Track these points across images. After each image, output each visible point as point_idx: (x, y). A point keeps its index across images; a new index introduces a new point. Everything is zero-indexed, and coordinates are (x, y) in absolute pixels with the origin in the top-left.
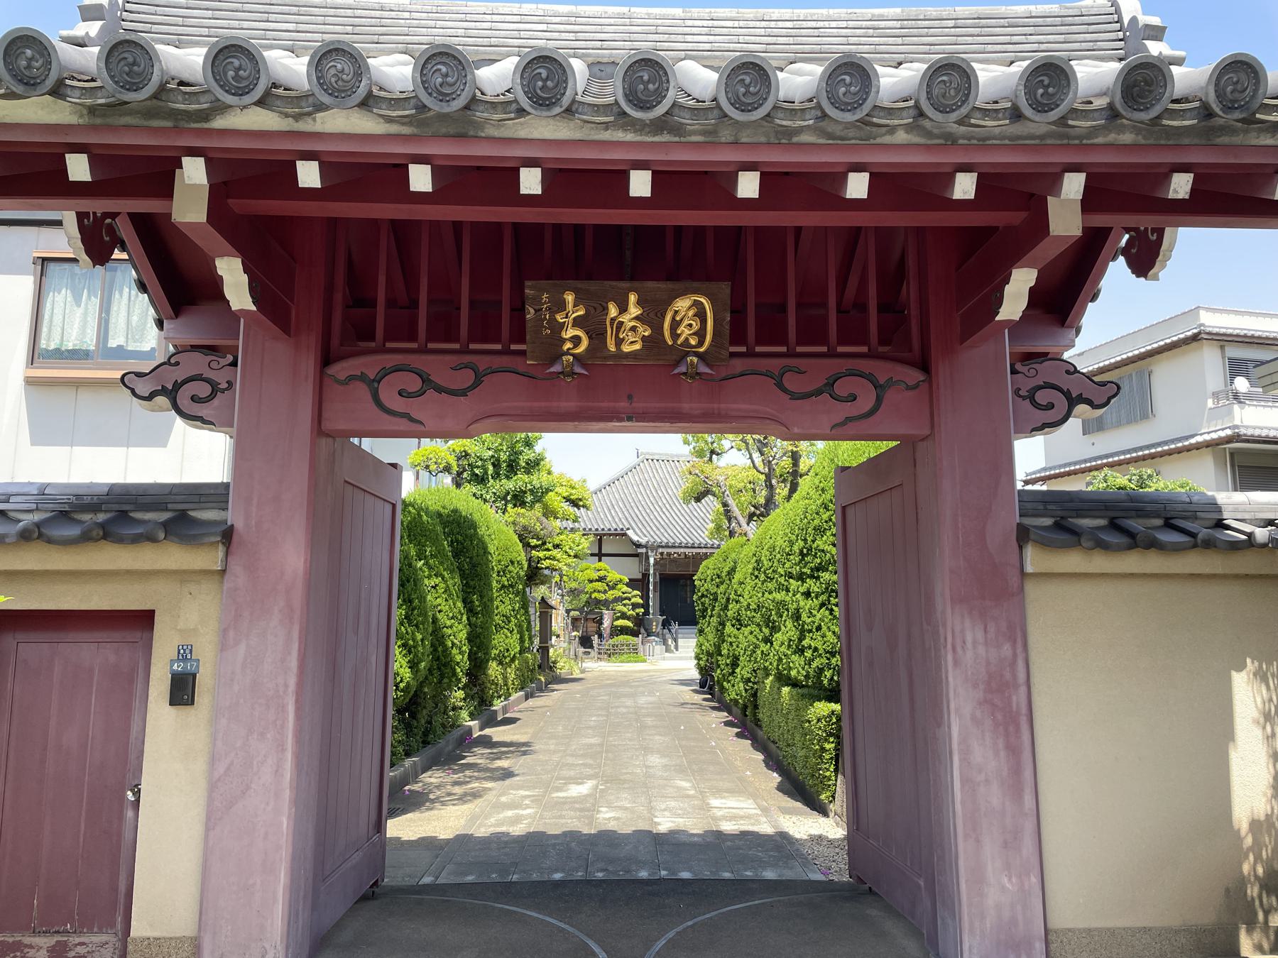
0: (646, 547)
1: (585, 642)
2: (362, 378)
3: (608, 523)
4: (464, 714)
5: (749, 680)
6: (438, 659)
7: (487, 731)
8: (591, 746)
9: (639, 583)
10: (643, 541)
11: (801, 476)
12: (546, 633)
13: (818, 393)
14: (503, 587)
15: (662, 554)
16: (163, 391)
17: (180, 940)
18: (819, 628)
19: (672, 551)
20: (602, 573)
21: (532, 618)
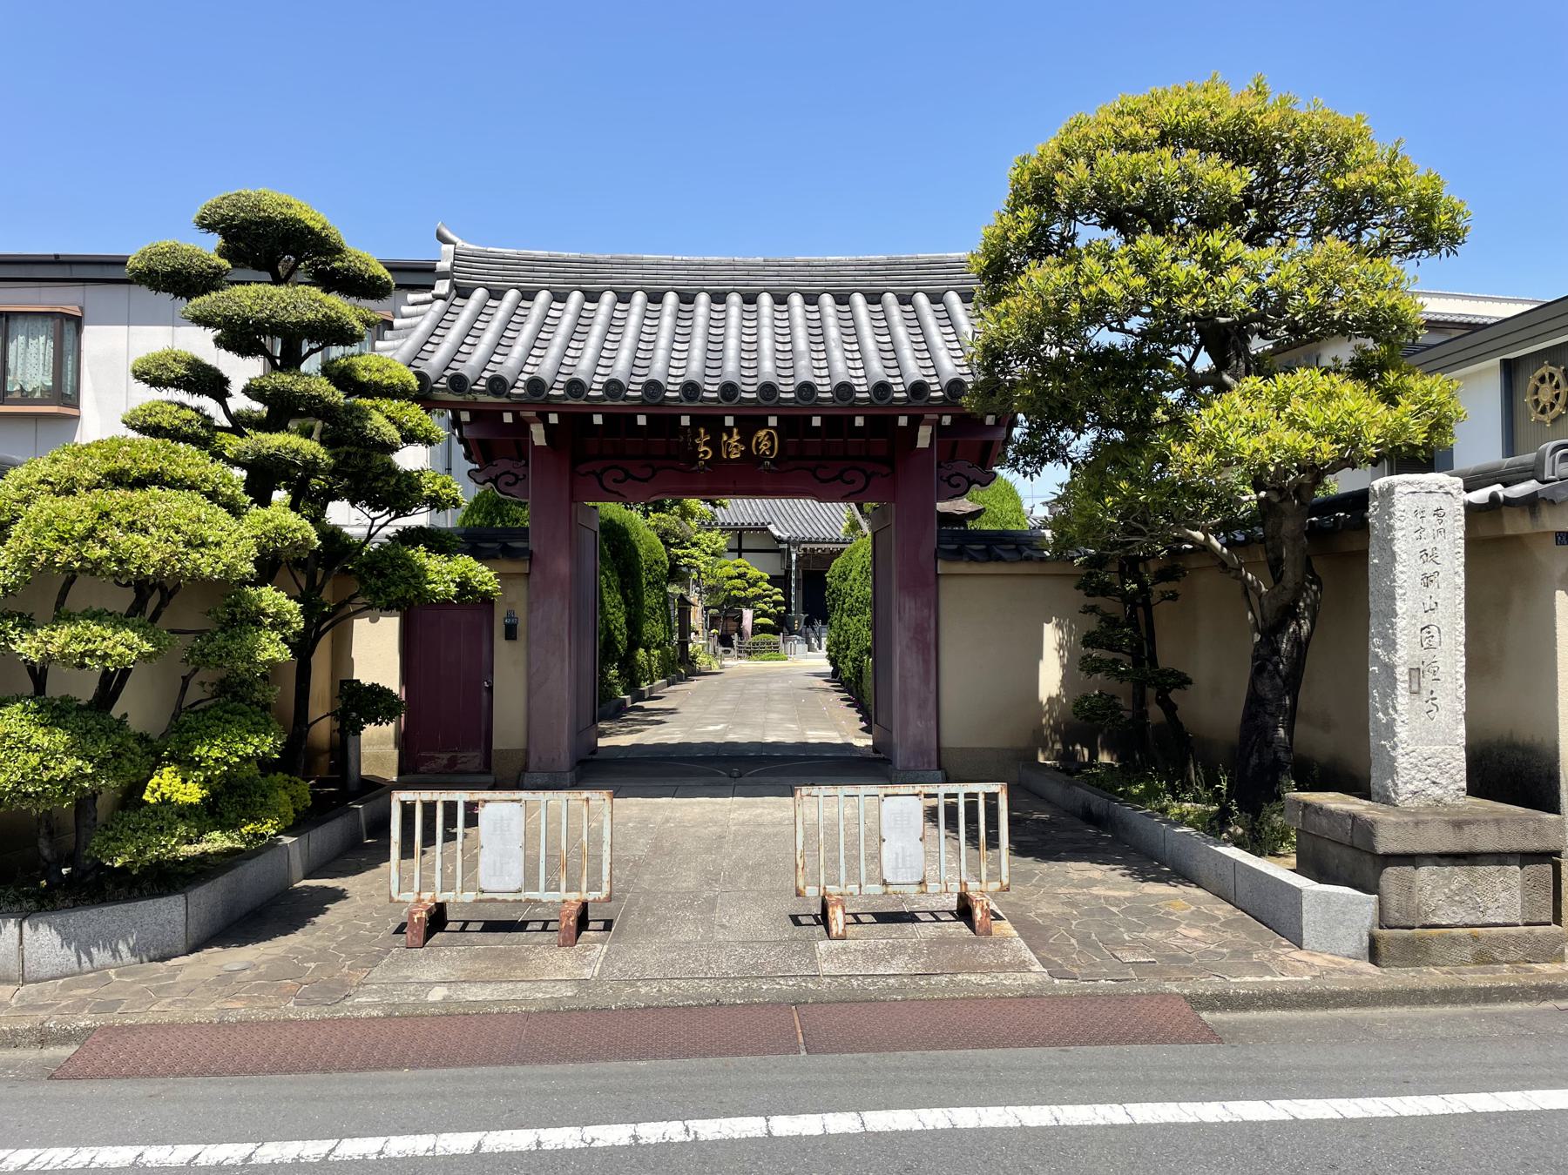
0: (787, 542)
1: (725, 641)
2: (594, 473)
10: (785, 536)
12: (685, 629)
13: (834, 479)
16: (490, 480)
17: (517, 750)
19: (816, 546)
20: (742, 570)
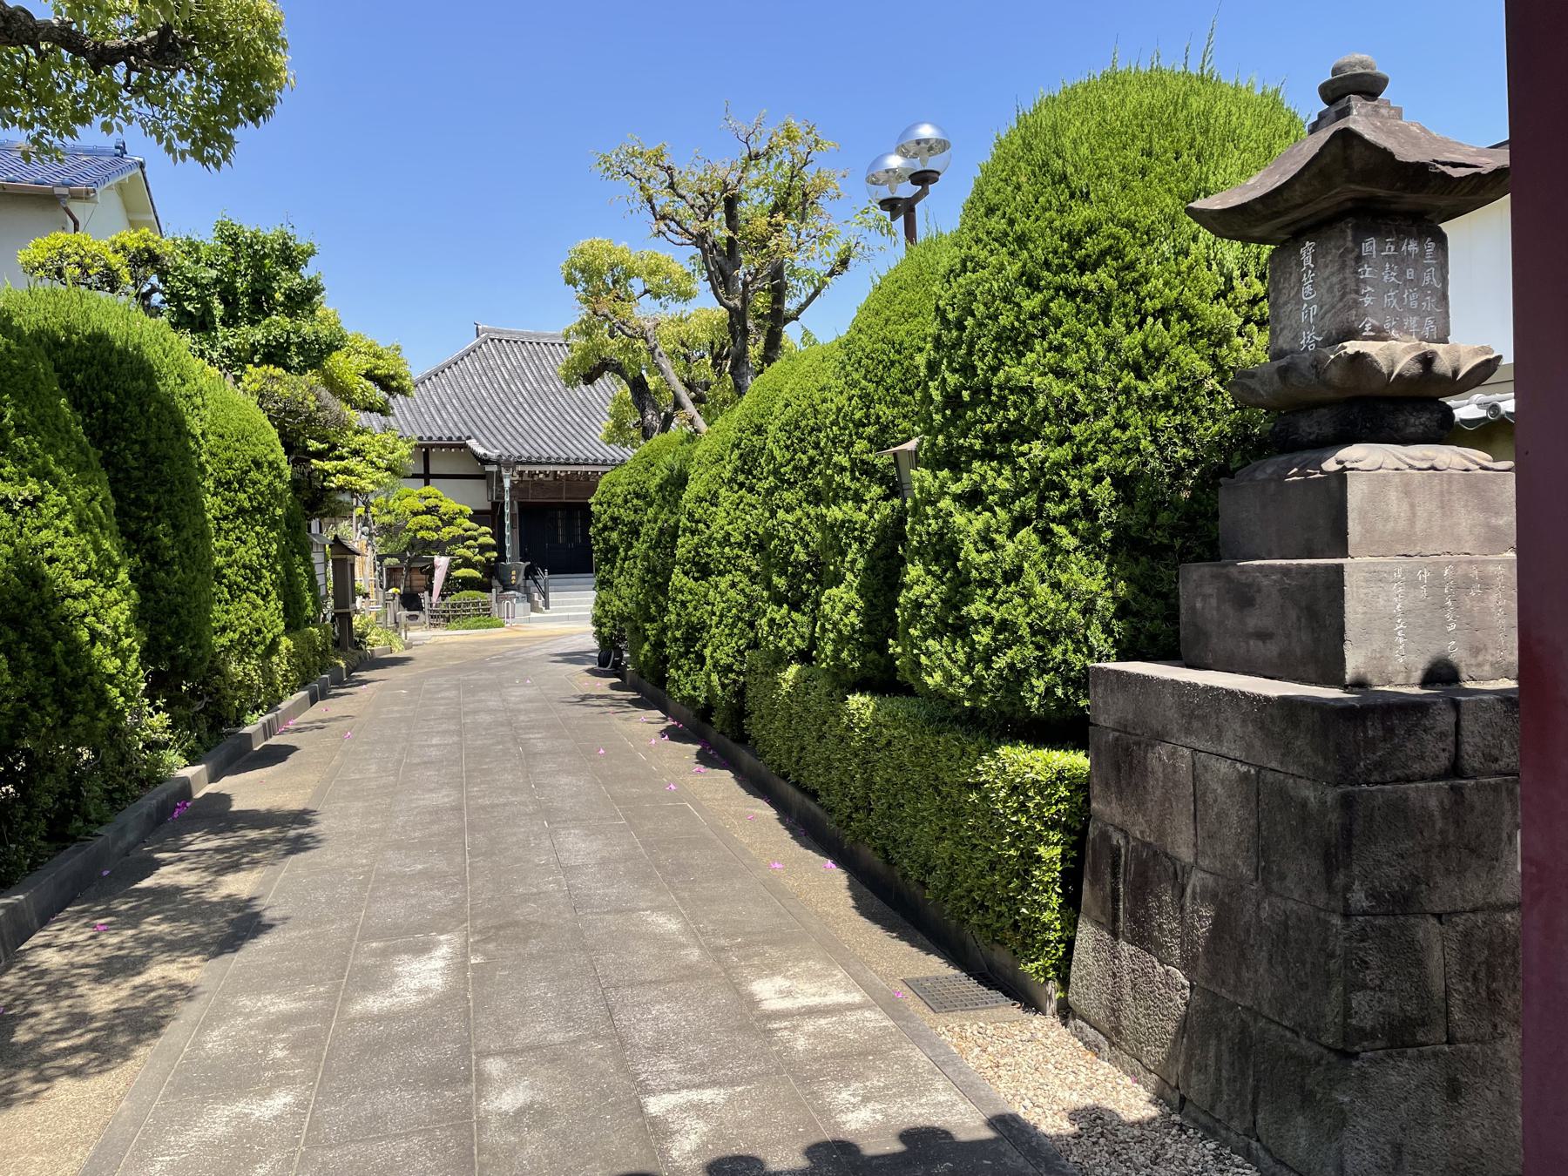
0: (497, 463)
1: (411, 601)
3: (440, 428)
4: (172, 757)
5: (729, 668)
6: (54, 671)
7: (226, 784)
8: (436, 813)
9: (490, 516)
10: (493, 454)
11: (787, 320)
12: (345, 591)
14: (241, 511)
15: (521, 473)
18: (1014, 575)
19: (537, 469)
20: (432, 502)
21: (319, 569)
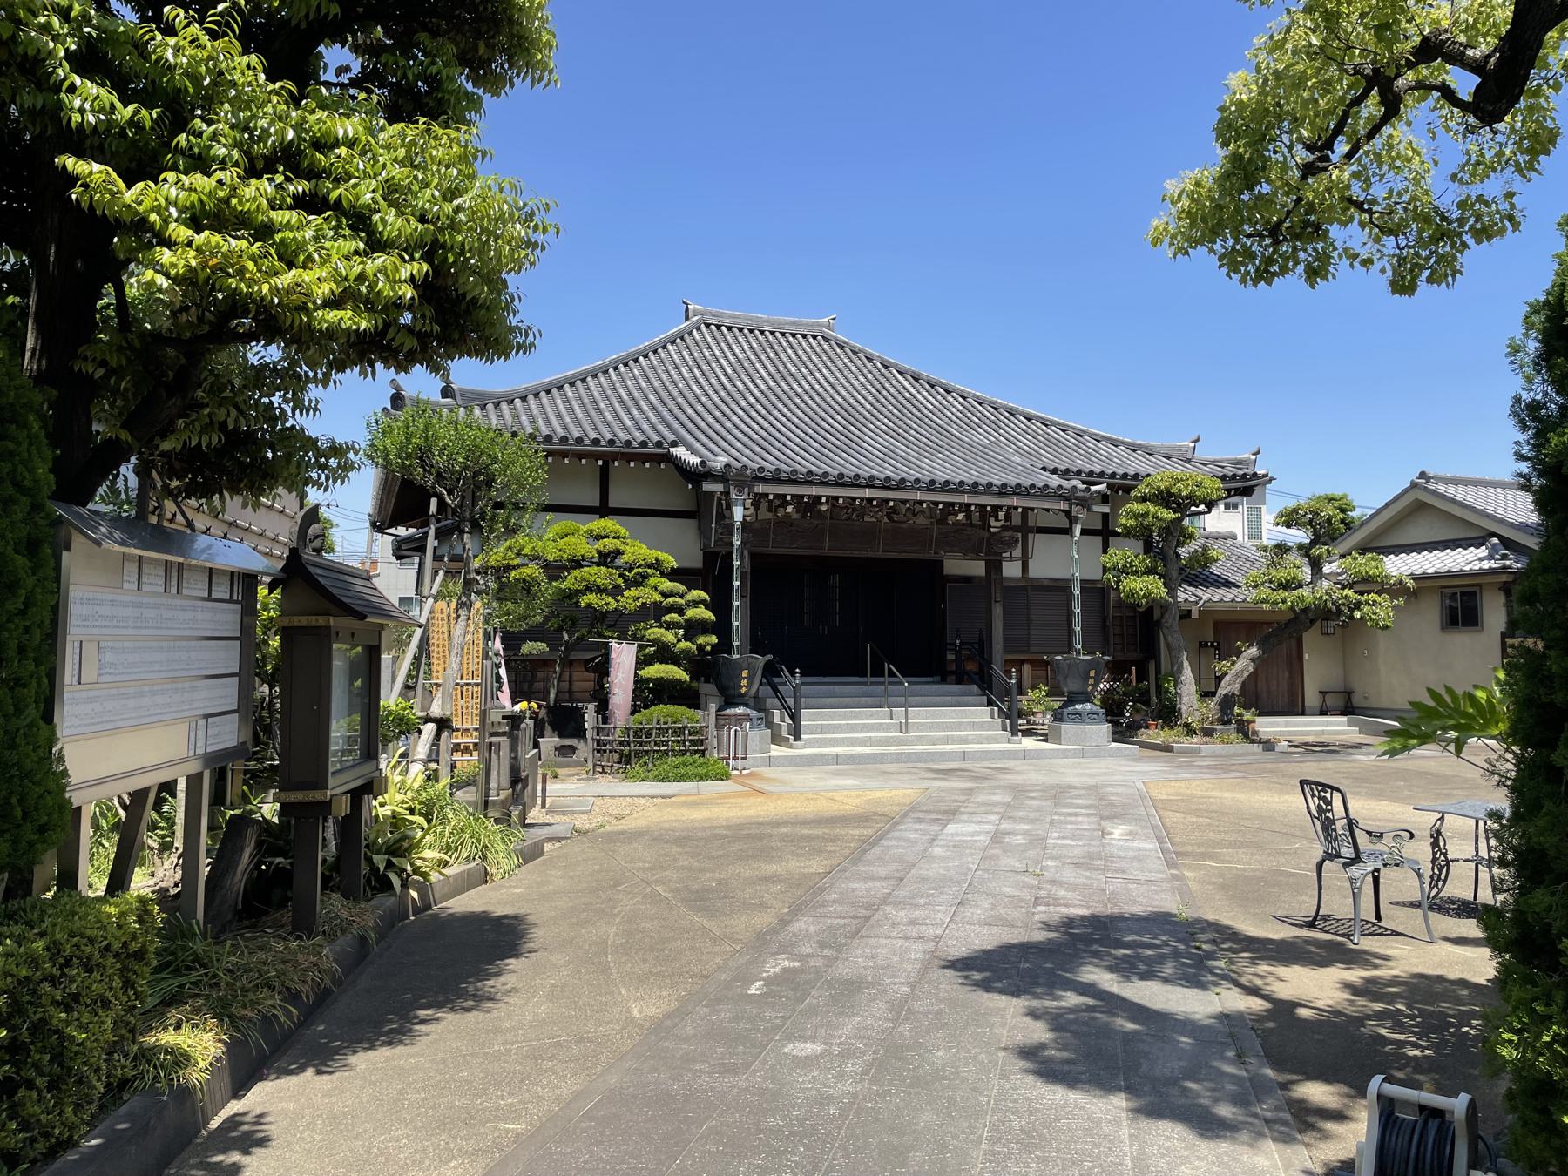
20: (608, 544)
